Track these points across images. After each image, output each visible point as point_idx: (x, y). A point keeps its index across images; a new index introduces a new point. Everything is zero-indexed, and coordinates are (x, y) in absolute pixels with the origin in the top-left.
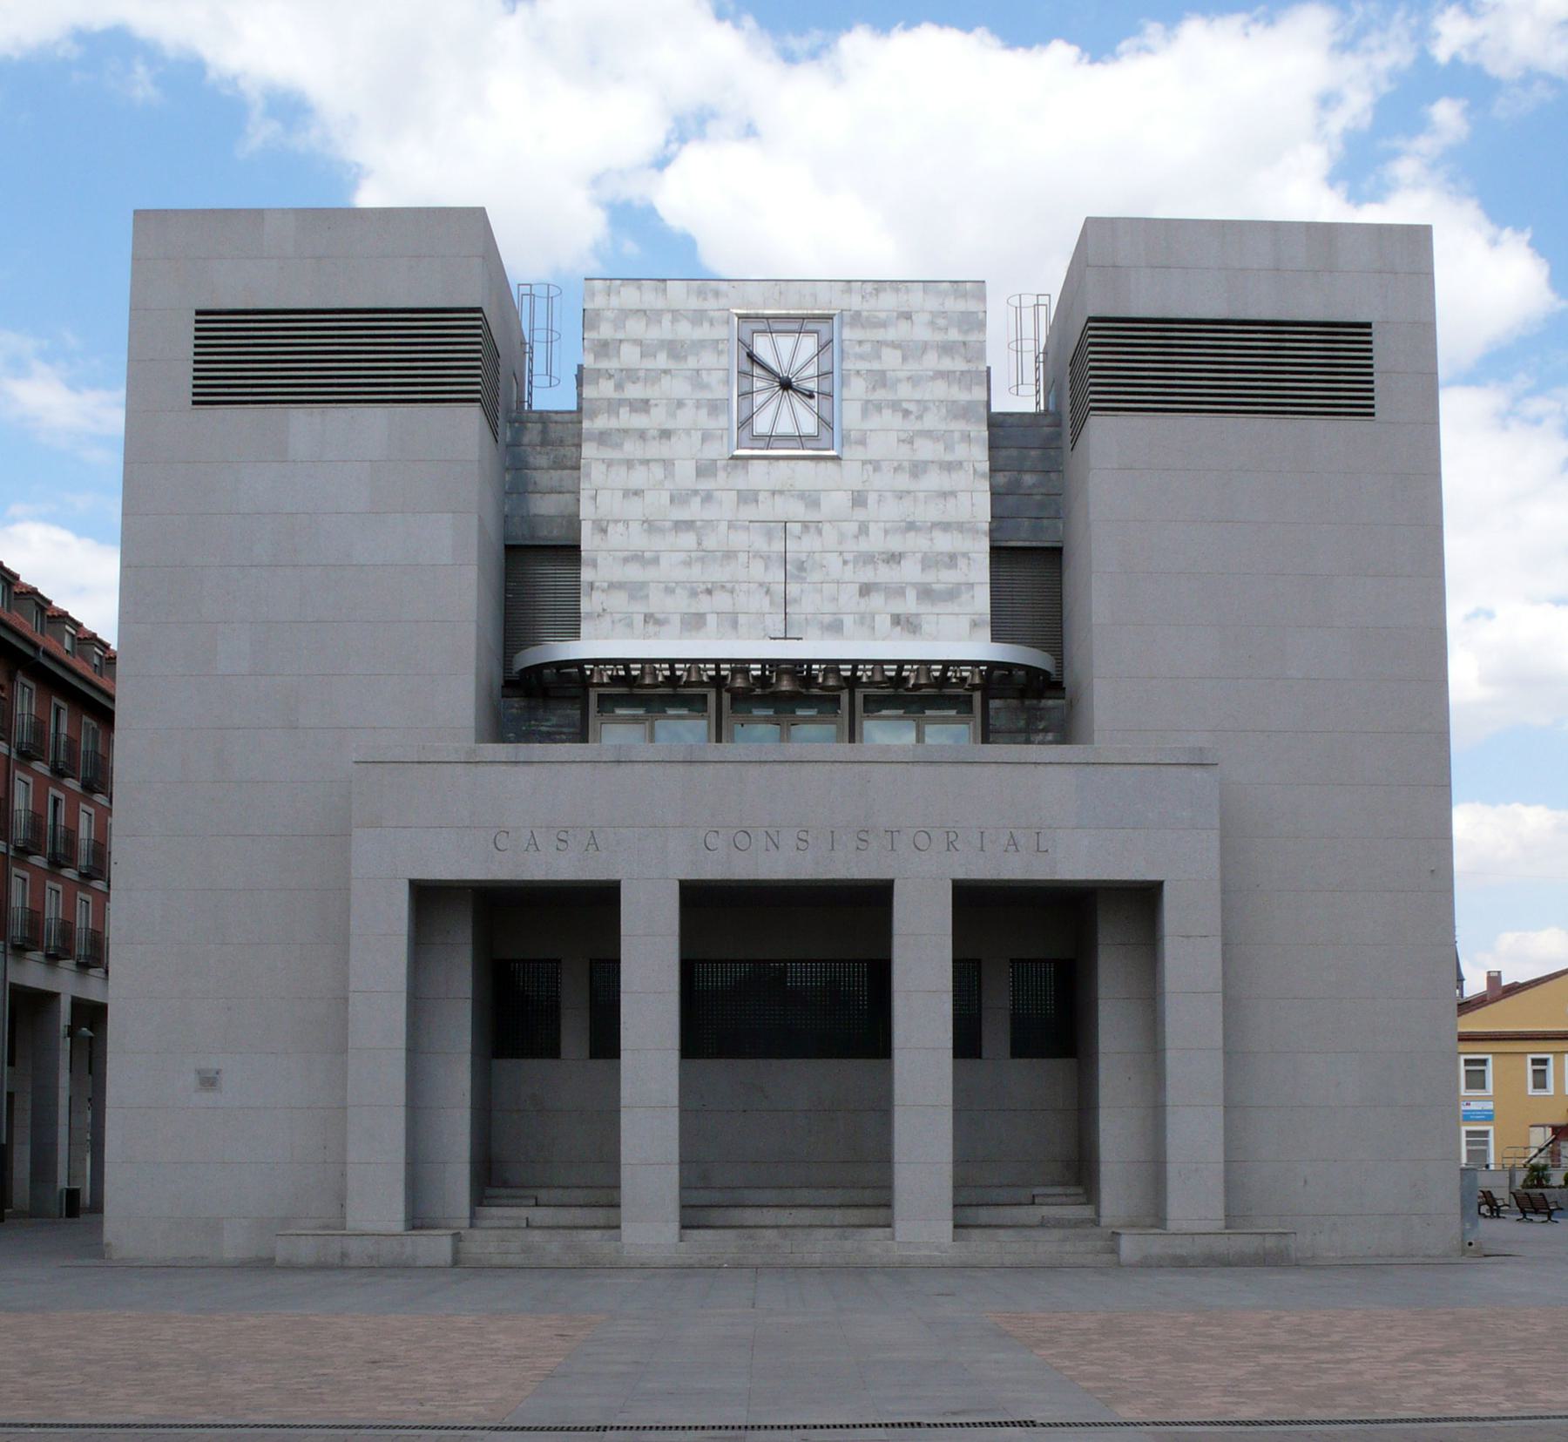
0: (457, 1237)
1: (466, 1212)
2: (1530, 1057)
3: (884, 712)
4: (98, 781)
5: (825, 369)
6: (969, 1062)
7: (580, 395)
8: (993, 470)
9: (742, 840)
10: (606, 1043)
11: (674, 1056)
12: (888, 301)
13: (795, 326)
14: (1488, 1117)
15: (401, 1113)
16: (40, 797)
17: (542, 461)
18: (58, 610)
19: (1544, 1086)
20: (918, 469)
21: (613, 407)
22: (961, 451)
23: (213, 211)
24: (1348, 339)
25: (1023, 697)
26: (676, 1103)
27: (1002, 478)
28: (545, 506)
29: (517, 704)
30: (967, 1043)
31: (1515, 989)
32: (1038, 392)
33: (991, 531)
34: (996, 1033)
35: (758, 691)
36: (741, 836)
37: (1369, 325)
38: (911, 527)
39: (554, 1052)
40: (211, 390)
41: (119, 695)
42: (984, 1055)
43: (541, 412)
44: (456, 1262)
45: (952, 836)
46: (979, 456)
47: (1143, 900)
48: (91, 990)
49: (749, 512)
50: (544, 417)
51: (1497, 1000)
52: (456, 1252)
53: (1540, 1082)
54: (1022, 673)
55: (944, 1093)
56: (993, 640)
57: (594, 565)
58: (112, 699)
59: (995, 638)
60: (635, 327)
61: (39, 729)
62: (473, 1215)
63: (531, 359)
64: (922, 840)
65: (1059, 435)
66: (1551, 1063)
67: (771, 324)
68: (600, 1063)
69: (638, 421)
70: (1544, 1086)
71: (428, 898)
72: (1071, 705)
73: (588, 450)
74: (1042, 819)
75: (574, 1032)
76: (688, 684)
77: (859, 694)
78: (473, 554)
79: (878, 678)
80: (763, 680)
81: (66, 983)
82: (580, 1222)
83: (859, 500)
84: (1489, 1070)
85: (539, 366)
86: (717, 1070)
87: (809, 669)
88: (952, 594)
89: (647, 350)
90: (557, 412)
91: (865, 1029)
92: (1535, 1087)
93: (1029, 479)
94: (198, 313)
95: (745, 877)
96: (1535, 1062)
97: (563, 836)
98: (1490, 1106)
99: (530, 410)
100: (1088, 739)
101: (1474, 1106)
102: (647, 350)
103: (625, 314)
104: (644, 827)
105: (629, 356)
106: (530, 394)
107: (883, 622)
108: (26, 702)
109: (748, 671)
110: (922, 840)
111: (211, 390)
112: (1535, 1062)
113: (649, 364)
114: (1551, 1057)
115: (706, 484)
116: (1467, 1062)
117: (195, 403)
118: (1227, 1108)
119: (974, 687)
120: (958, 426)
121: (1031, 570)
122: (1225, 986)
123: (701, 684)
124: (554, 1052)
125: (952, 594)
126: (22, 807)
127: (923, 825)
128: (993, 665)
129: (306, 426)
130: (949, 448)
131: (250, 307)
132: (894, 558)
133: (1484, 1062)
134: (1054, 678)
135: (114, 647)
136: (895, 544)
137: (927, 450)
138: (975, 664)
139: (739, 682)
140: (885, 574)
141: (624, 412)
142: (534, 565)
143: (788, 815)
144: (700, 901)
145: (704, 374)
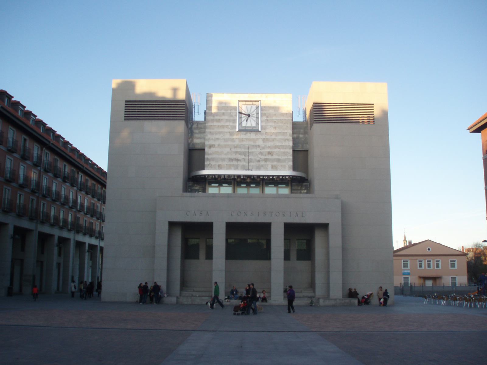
0: (177, 298)
1: (179, 292)
2: (403, 260)
3: (270, 186)
4: (102, 199)
5: (257, 112)
6: (287, 262)
7: (205, 117)
8: (293, 133)
9: (239, 214)
10: (209, 256)
11: (224, 259)
13: (247, 128)
14: (409, 274)
15: (166, 271)
16: (40, 177)
17: (196, 131)
18: (87, 158)
19: (438, 267)
21: (213, 121)
25: (299, 182)
27: (295, 136)
28: (196, 141)
29: (191, 183)
30: (287, 257)
31: (415, 244)
32: (303, 116)
33: (293, 147)
34: (293, 255)
35: (243, 181)
37: (373, 104)
39: (197, 257)
41: (107, 183)
42: (291, 259)
43: (197, 121)
44: (177, 303)
45: (284, 213)
46: (290, 131)
47: (325, 227)
48: (102, 244)
50: (198, 123)
51: (411, 247)
52: (177, 301)
53: (421, 266)
54: (299, 177)
55: (282, 268)
56: (293, 171)
58: (106, 183)
59: (293, 170)
61: (40, 158)
62: (180, 293)
63: (194, 109)
64: (277, 214)
65: (307, 126)
66: (423, 261)
68: (208, 261)
70: (454, 267)
71: (172, 225)
72: (310, 184)
73: (207, 130)
75: (202, 253)
76: (228, 180)
78: (182, 153)
79: (268, 179)
80: (244, 179)
81: (88, 240)
84: (409, 263)
85: (196, 110)
87: (254, 177)
88: (284, 161)
90: (200, 121)
91: (265, 254)
92: (428, 267)
93: (301, 136)
94: (126, 101)
96: (419, 261)
98: (409, 271)
99: (194, 121)
100: (313, 193)
101: (405, 271)
104: (218, 208)
106: (194, 116)
107: (270, 167)
108: (11, 134)
109: (240, 177)
110: (277, 214)
111: (127, 118)
112: (428, 261)
114: (432, 260)
116: (404, 261)
117: (125, 120)
118: (343, 272)
119: (289, 181)
121: (301, 156)
122: (342, 245)
123: (230, 179)
124: (197, 257)
125: (284, 161)
126: (9, 166)
127: (278, 209)
128: (293, 176)
133: (407, 261)
134: (306, 178)
135: (107, 172)
138: (289, 176)
139: (239, 180)
142: (194, 156)
143: (251, 206)
145: (232, 114)
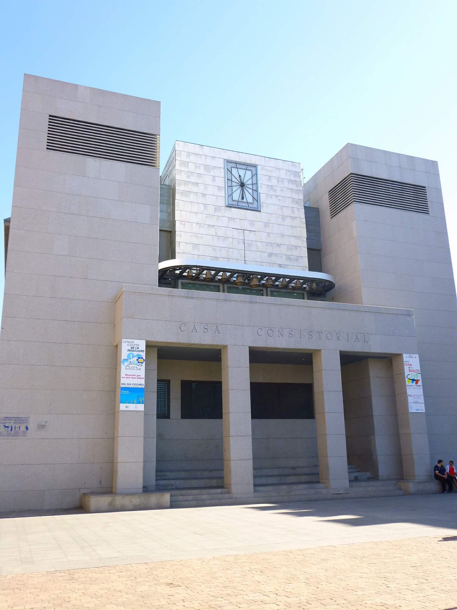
12: (272, 163)
13: (245, 167)
20: (284, 218)
22: (296, 214)
23: (58, 81)
24: (419, 191)
26: (251, 434)
36: (270, 331)
38: (283, 236)
40: (53, 145)
49: (232, 225)
57: (181, 236)
60: (193, 158)
67: (237, 164)
69: (195, 189)
74: (319, 332)
77: (269, 290)
82: (194, 486)
83: (266, 225)
86: (257, 421)
89: (197, 166)
94: (50, 116)
95: (272, 346)
97: (206, 327)
102: (197, 166)
103: (189, 154)
105: (192, 167)
113: (198, 171)
115: (219, 214)
117: (47, 148)
120: (296, 206)
129: (93, 165)
130: (293, 212)
131: (72, 118)
132: (279, 245)
136: (279, 241)
137: (287, 212)
140: (276, 250)
141: (190, 185)
144: (257, 356)
